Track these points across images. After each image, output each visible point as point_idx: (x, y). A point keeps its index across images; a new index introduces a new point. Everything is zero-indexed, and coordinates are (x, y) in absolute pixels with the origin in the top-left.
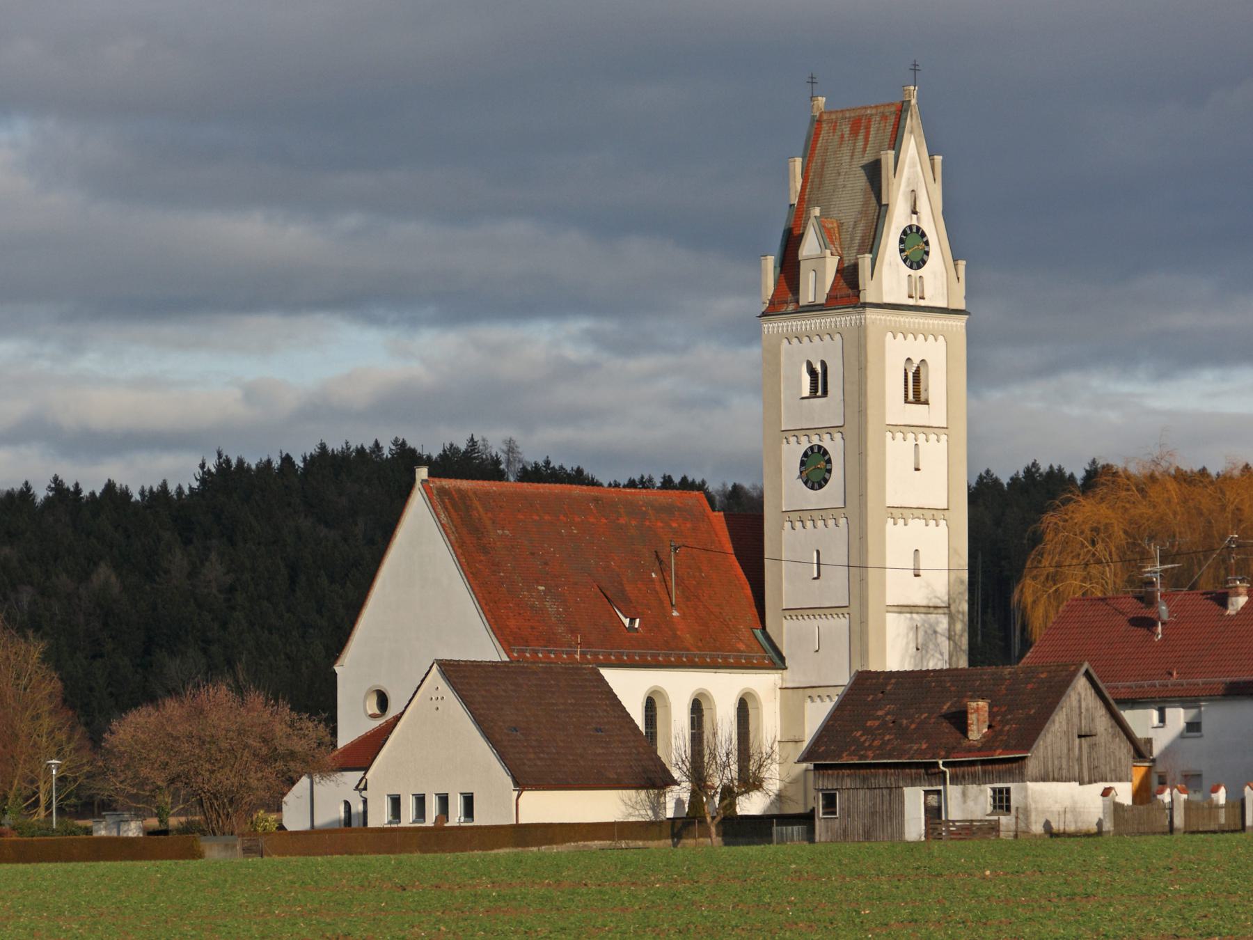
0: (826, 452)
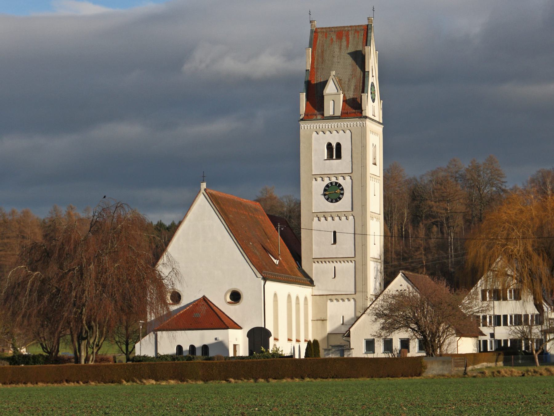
0: (340, 185)
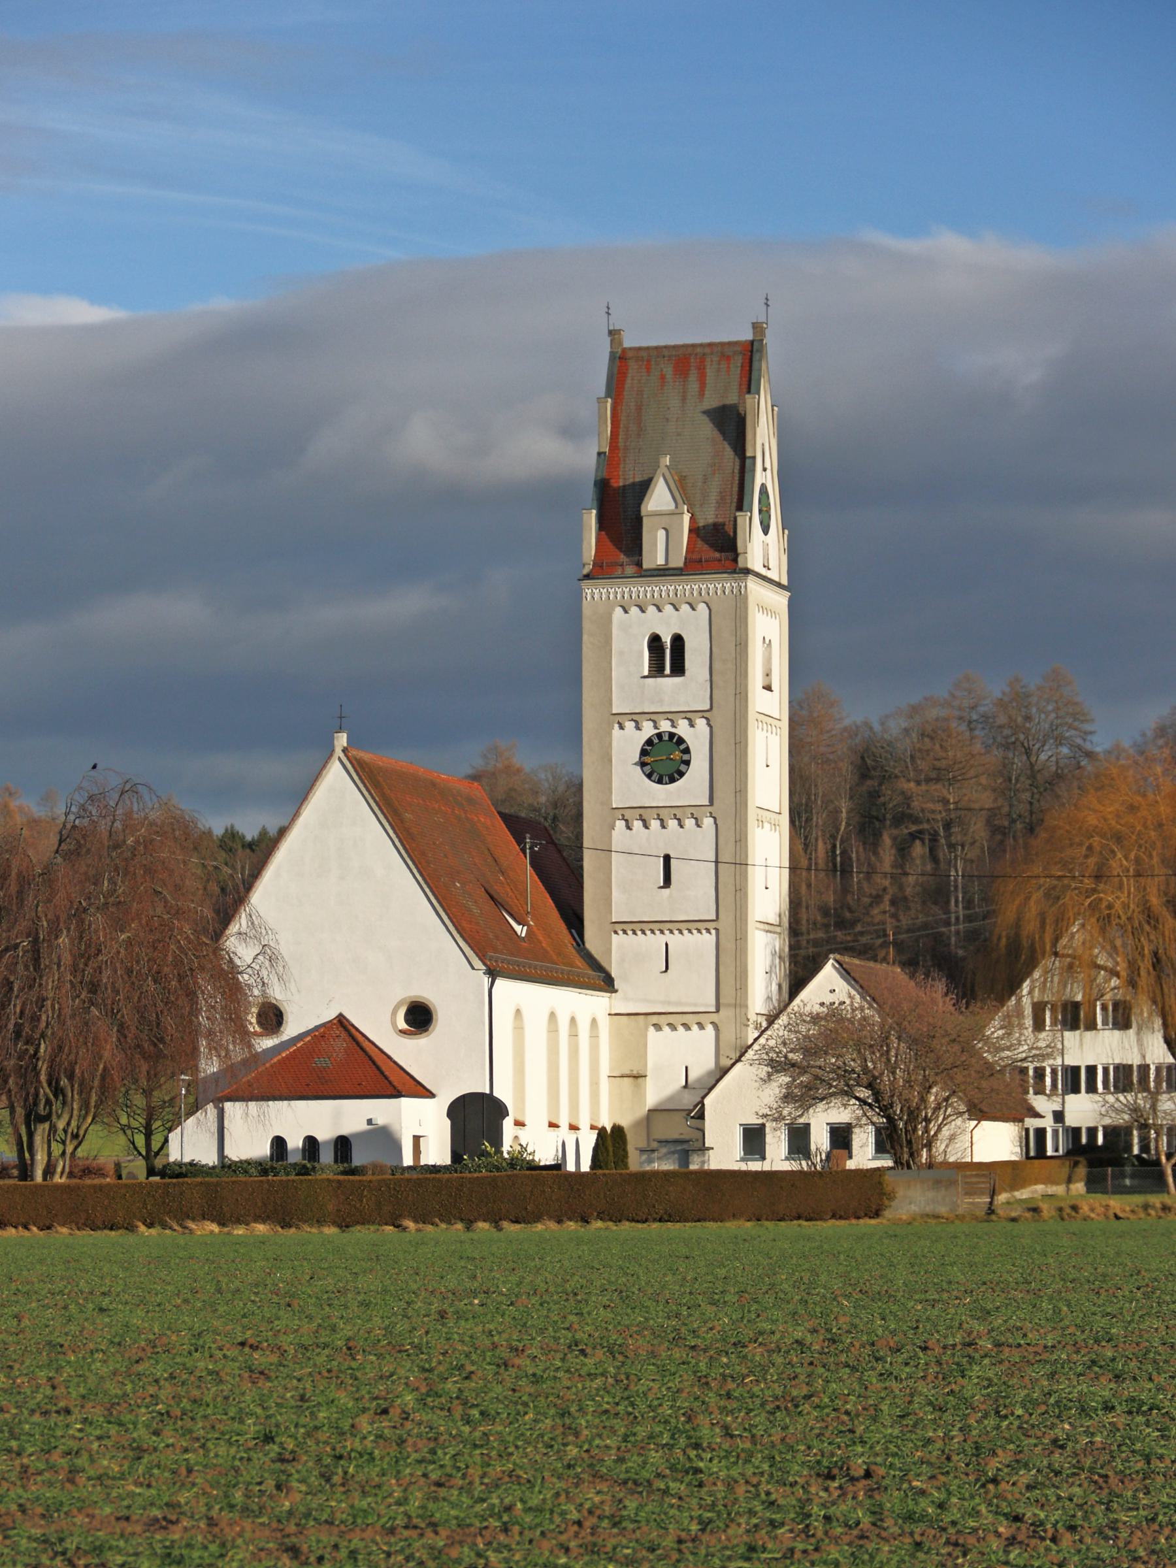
0: (681, 741)
